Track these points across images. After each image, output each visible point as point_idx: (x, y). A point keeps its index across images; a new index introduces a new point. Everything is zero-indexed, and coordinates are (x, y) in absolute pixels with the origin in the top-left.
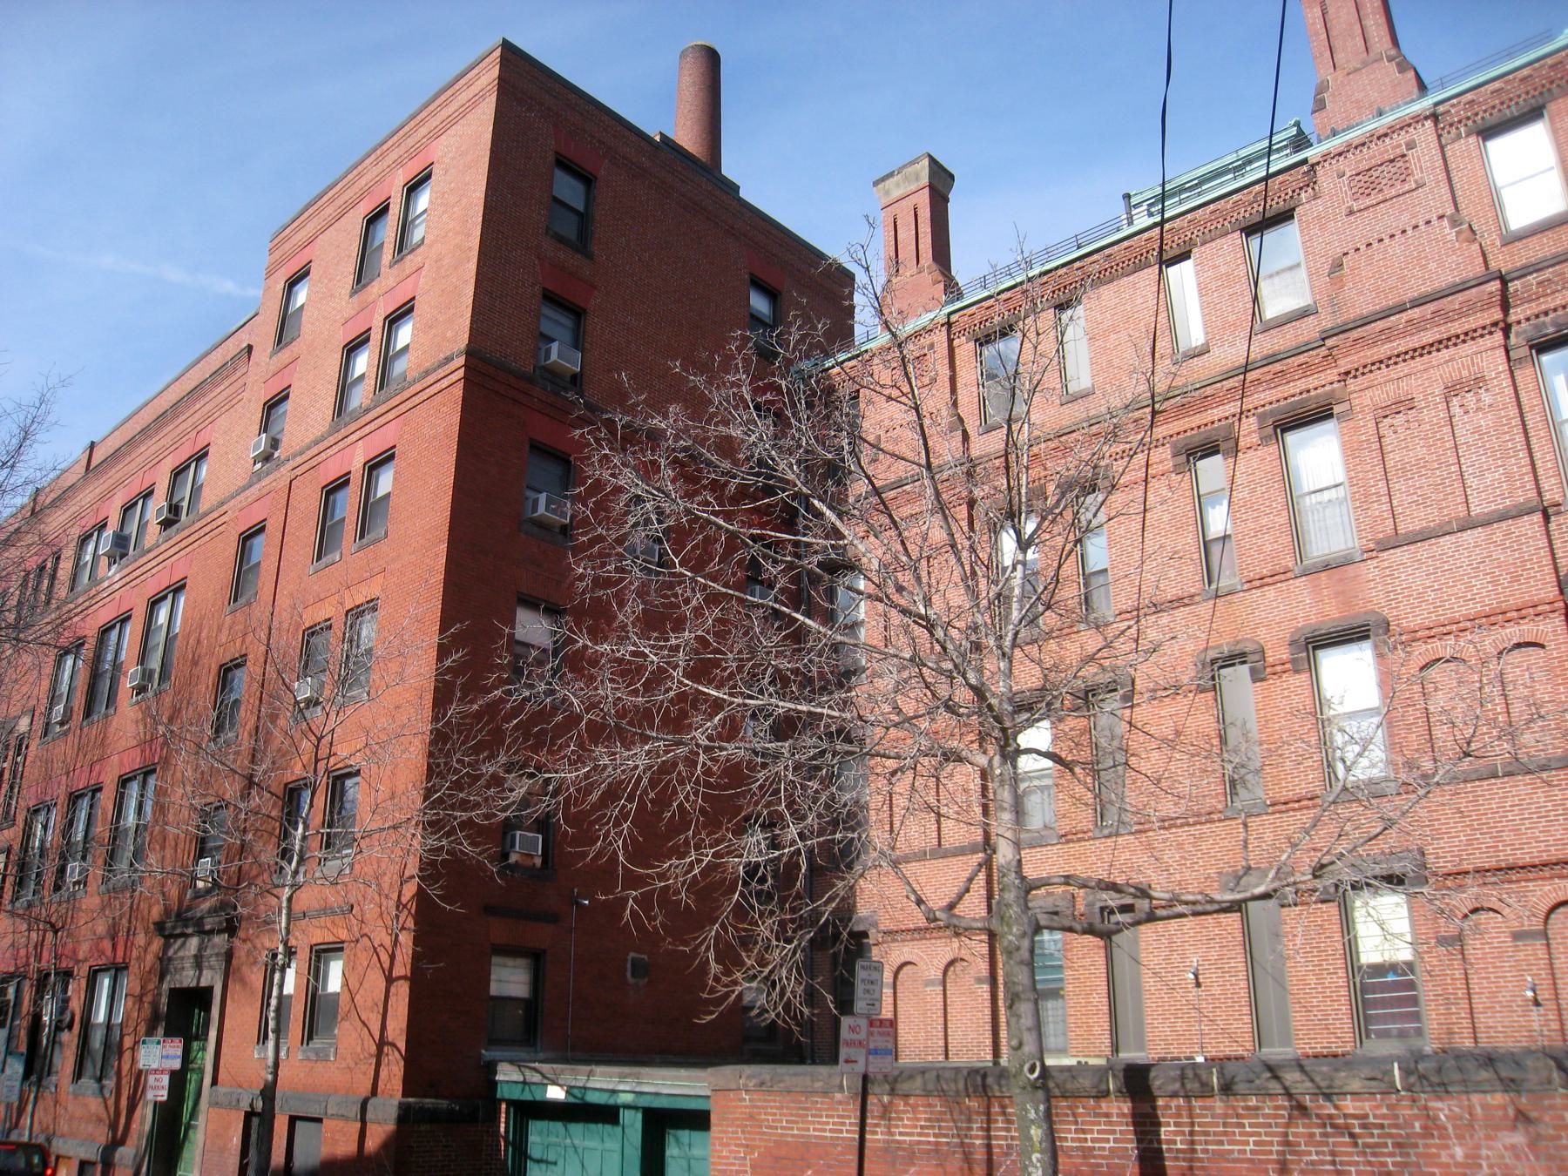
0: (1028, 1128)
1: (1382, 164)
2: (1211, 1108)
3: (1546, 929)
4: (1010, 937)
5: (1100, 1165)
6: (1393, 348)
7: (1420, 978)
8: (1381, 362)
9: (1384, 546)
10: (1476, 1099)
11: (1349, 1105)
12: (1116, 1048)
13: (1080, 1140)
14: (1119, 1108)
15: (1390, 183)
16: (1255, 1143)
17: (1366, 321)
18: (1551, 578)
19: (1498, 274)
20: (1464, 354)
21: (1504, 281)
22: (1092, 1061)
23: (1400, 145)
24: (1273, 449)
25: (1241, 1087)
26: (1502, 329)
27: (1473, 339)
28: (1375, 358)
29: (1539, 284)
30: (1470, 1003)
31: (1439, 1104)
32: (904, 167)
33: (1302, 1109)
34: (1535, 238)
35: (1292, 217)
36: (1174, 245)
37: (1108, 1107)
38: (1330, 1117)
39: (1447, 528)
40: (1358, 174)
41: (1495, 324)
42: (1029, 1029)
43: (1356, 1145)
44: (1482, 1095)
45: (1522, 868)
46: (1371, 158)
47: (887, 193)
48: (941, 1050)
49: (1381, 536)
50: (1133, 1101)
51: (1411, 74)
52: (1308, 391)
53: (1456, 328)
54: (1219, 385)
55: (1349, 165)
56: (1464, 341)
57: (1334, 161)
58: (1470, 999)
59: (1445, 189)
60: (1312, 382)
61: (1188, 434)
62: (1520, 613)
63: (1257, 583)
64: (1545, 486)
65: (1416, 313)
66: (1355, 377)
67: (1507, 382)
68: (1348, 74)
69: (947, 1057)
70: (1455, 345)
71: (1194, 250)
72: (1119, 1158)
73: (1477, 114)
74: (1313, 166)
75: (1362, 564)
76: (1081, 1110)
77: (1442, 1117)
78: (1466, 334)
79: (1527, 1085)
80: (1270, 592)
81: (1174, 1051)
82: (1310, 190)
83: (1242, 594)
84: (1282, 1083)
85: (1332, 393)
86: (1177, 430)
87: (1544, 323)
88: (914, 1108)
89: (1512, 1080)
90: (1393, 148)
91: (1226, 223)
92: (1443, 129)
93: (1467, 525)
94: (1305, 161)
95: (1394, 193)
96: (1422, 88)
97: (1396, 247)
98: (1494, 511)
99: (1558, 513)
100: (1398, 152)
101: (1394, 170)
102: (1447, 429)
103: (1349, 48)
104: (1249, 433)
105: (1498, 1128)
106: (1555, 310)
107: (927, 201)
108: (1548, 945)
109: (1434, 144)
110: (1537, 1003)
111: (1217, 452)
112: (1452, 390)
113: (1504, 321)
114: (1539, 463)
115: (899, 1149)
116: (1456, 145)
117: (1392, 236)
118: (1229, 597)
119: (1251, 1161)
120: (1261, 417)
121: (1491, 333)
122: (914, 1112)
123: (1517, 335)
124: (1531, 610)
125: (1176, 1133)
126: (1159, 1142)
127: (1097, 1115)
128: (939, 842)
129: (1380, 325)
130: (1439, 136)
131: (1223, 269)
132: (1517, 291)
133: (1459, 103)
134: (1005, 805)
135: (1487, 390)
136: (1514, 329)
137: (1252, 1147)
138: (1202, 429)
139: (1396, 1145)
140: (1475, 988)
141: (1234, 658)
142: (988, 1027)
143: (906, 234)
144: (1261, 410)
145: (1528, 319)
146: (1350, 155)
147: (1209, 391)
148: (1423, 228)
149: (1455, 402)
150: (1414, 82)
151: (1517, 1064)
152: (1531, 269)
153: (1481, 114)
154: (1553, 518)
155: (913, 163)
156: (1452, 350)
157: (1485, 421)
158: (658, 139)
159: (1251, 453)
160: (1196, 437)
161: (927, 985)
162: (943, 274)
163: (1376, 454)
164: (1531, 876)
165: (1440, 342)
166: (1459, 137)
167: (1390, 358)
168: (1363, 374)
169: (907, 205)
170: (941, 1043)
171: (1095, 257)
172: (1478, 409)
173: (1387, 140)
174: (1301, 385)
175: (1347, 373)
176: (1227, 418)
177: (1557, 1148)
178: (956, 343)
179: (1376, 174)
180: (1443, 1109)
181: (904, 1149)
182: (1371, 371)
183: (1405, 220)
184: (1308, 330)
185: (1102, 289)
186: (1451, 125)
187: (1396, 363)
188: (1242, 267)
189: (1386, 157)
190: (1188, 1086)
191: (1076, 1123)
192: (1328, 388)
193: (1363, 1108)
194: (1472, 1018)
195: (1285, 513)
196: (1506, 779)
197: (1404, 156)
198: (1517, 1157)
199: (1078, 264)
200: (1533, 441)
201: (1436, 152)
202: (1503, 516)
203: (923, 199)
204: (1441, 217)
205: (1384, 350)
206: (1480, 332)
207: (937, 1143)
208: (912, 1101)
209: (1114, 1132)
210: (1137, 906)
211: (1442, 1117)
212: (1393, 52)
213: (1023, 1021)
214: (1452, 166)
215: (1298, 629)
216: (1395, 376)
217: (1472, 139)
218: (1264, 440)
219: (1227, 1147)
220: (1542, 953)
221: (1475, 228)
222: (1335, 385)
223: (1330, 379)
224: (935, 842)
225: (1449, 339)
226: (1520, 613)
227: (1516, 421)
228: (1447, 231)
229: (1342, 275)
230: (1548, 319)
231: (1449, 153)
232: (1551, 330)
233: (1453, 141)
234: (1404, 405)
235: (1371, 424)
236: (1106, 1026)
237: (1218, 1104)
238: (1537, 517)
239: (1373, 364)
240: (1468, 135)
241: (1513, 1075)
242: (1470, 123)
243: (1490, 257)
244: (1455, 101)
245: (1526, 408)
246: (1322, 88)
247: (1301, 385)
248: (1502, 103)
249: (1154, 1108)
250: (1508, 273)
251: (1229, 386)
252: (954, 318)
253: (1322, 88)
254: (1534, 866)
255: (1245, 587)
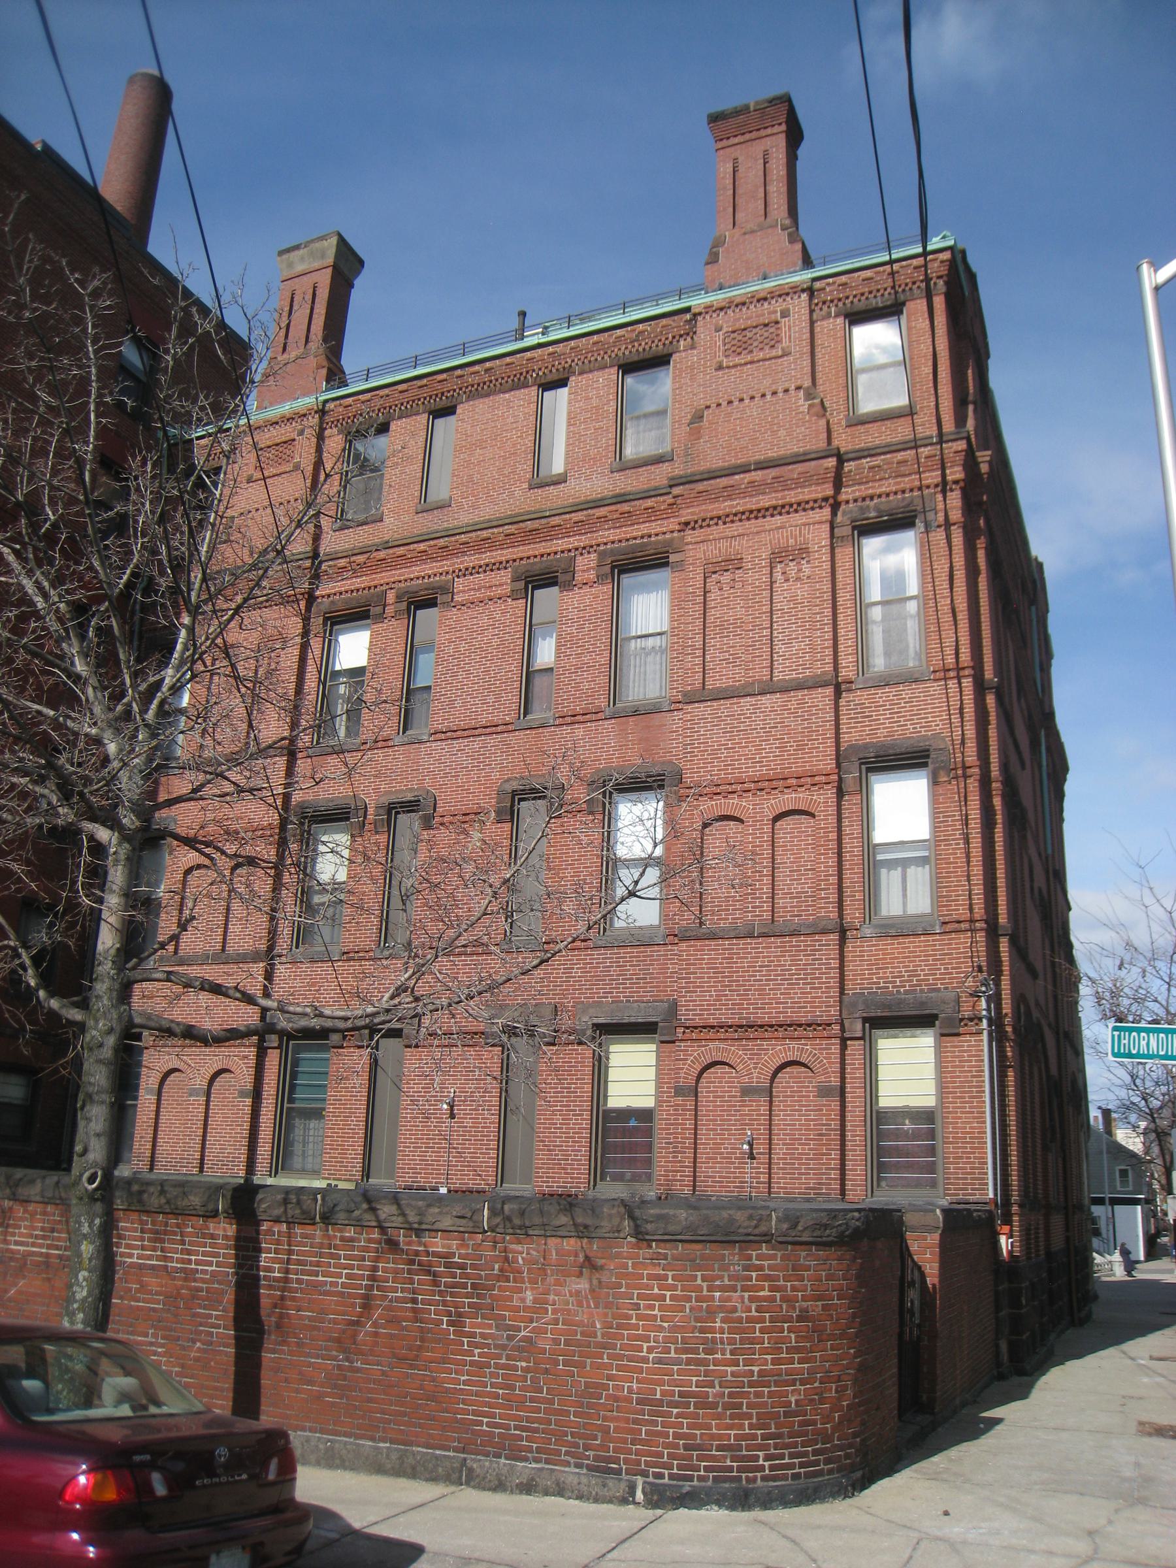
0: (79, 1243)
1: (756, 327)
2: (313, 1237)
3: (771, 1087)
4: (94, 1033)
5: (200, 1290)
6: (732, 507)
7: (659, 1124)
8: (719, 518)
9: (691, 699)
10: (552, 1242)
11: (438, 1244)
12: (367, 1173)
13: (183, 1261)
14: (225, 1230)
15: (761, 346)
16: (348, 1276)
17: (712, 475)
18: (831, 751)
19: (835, 452)
20: (794, 523)
21: (841, 459)
22: (342, 1185)
23: (776, 312)
24: (607, 588)
25: (341, 1217)
26: (831, 505)
27: (804, 510)
28: (715, 513)
29: (871, 468)
30: (695, 1153)
31: (518, 1247)
32: (312, 241)
33: (393, 1244)
34: (876, 424)
35: (668, 363)
36: (554, 370)
37: (215, 1228)
38: (417, 1253)
39: (750, 691)
40: (734, 332)
41: (825, 499)
42: (98, 1135)
43: (436, 1283)
44: (559, 1240)
45: (761, 1026)
46: (748, 319)
47: (290, 265)
48: (196, 1163)
49: (689, 688)
50: (238, 1224)
51: (798, 246)
52: (650, 536)
53: (792, 496)
54: (568, 516)
55: (727, 321)
56: (796, 511)
57: (714, 315)
58: (695, 1149)
59: (807, 363)
60: (654, 527)
61: (531, 561)
62: (800, 780)
63: (569, 720)
64: (843, 663)
65: (757, 475)
66: (693, 529)
67: (826, 557)
68: (745, 234)
69: (201, 1170)
70: (788, 513)
71: (572, 378)
72: (219, 1283)
73: (847, 298)
74: (695, 315)
75: (669, 715)
76: (190, 1230)
77: (520, 1261)
78: (799, 504)
79: (601, 1232)
80: (579, 731)
81: (421, 1181)
82: (689, 339)
83: (553, 729)
84: (377, 1216)
85: (669, 543)
86: (520, 555)
87: (868, 506)
88: (33, 1214)
89: (586, 1227)
90: (769, 313)
91: (606, 357)
92: (817, 305)
93: (768, 689)
94: (687, 310)
95: (761, 355)
96: (808, 262)
97: (753, 409)
98: (794, 679)
99: (849, 690)
100: (773, 317)
101: (766, 334)
102: (766, 593)
103: (750, 210)
104: (588, 570)
105: (567, 1274)
106: (880, 496)
107: (328, 281)
108: (771, 1102)
109: (806, 317)
110: (752, 1157)
111: (555, 584)
112: (778, 556)
113: (834, 497)
114: (841, 640)
115: (11, 1259)
116: (825, 323)
117: (752, 398)
118: (540, 730)
119: (342, 1294)
120: (602, 555)
121: (821, 507)
122: (32, 1220)
123: (844, 513)
124: (809, 779)
125: (274, 1260)
126: (258, 1268)
127: (204, 1236)
128: (224, 947)
129: (724, 481)
130: (812, 311)
131: (595, 402)
132: (850, 471)
133: (834, 283)
134: (115, 887)
135: (808, 562)
136: (843, 507)
137: (343, 1280)
138: (545, 558)
139: (474, 1286)
140: (702, 1139)
141: (535, 794)
142: (245, 1142)
143: (301, 315)
144: (602, 548)
145: (855, 501)
146: (730, 312)
147: (556, 520)
148: (781, 395)
149: (779, 567)
150: (799, 255)
151: (593, 1210)
152: (866, 453)
153: (851, 298)
154: (844, 694)
155: (322, 238)
156: (784, 518)
157: (801, 591)
158: (39, 147)
159: (586, 589)
160: (538, 565)
161: (191, 1095)
162: (328, 359)
163: (700, 607)
164: (767, 1035)
165: (775, 508)
166: (829, 315)
167: (727, 516)
168: (701, 527)
169: (308, 281)
170: (197, 1155)
171: (477, 368)
172: (798, 579)
173: (766, 304)
174: (644, 529)
175: (687, 524)
176: (570, 551)
177: (615, 1296)
178: (327, 432)
179: (749, 335)
180: (523, 1252)
181: (17, 1260)
182: (709, 526)
183: (766, 385)
184: (659, 476)
185: (476, 402)
186: (824, 303)
187: (732, 522)
188: (613, 403)
189: (761, 320)
190: (290, 1213)
191: (183, 1242)
192: (668, 536)
193: (449, 1247)
194: (695, 1167)
195: (606, 653)
196: (760, 940)
197: (777, 322)
198: (580, 1304)
199: (459, 372)
200: (840, 617)
201: (805, 325)
202: (800, 686)
203: (324, 279)
204: (798, 388)
205: (725, 506)
206: (811, 504)
207: (47, 1255)
208: (31, 1208)
209: (216, 1255)
210: (405, 1031)
211: (520, 1261)
212: (787, 222)
213: (93, 1125)
214: (818, 342)
215: (598, 770)
216: (730, 534)
217: (840, 320)
218: (600, 579)
219: (320, 1278)
220: (764, 1109)
221: (827, 404)
222: (675, 534)
223: (671, 527)
224: (218, 947)
225: (783, 506)
226: (800, 780)
227: (828, 596)
228: (801, 402)
229: (701, 427)
230: (872, 504)
231: (817, 329)
232: (873, 514)
233: (823, 319)
234: (733, 564)
235: (700, 577)
236: (360, 1150)
237: (318, 1232)
238: (829, 691)
239: (712, 519)
240: (837, 316)
241: (589, 1222)
242: (840, 304)
243: (834, 435)
244: (831, 280)
245: (839, 585)
246: (718, 242)
247: (644, 529)
248: (870, 292)
249: (258, 1232)
250: (846, 453)
251: (576, 519)
252: (331, 406)
253: (718, 242)
254: (771, 1026)
255: (557, 722)
